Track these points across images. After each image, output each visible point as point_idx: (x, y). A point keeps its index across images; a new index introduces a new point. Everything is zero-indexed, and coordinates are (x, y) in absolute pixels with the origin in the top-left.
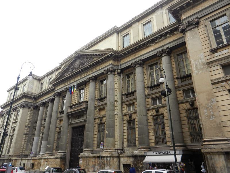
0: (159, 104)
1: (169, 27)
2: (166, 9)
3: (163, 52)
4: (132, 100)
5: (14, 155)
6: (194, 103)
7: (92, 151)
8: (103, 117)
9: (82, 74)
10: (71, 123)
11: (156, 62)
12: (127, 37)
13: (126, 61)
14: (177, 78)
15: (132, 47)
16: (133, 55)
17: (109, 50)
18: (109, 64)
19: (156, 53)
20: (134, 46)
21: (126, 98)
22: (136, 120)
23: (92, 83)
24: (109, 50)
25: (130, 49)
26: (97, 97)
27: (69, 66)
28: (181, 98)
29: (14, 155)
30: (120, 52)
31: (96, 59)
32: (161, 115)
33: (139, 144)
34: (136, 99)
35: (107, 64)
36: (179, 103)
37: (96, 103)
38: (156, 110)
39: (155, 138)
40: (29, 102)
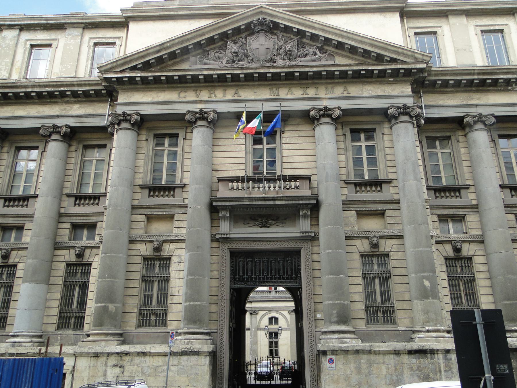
0: (87, 239)
1: (483, 72)
2: (27, 38)
3: (56, 130)
4: (460, 208)
5: (185, 333)
6: (10, 253)
7: (121, 335)
8: (165, 241)
9: (279, 87)
10: (232, 236)
11: (448, 134)
12: (45, 51)
13: (441, 103)
14: (467, 187)
15: (474, 74)
16: (464, 95)
17: (420, 56)
18: (399, 94)
19: (39, 126)
20: (479, 74)
21: (4, 206)
22: (20, 266)
23: (129, 132)
24: (420, 56)
25: (501, 77)
26: (144, 177)
27: (224, 37)
28: (65, 239)
29: (185, 333)
30: (433, 73)
31: (341, 62)
32: (465, 258)
33: (99, 323)
34: (31, 216)
35: (394, 90)
36: (57, 247)
37: (138, 196)
38: (76, 251)
39: (60, 313)
40: (512, 91)
